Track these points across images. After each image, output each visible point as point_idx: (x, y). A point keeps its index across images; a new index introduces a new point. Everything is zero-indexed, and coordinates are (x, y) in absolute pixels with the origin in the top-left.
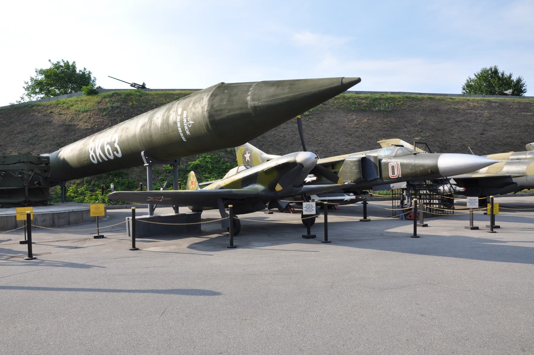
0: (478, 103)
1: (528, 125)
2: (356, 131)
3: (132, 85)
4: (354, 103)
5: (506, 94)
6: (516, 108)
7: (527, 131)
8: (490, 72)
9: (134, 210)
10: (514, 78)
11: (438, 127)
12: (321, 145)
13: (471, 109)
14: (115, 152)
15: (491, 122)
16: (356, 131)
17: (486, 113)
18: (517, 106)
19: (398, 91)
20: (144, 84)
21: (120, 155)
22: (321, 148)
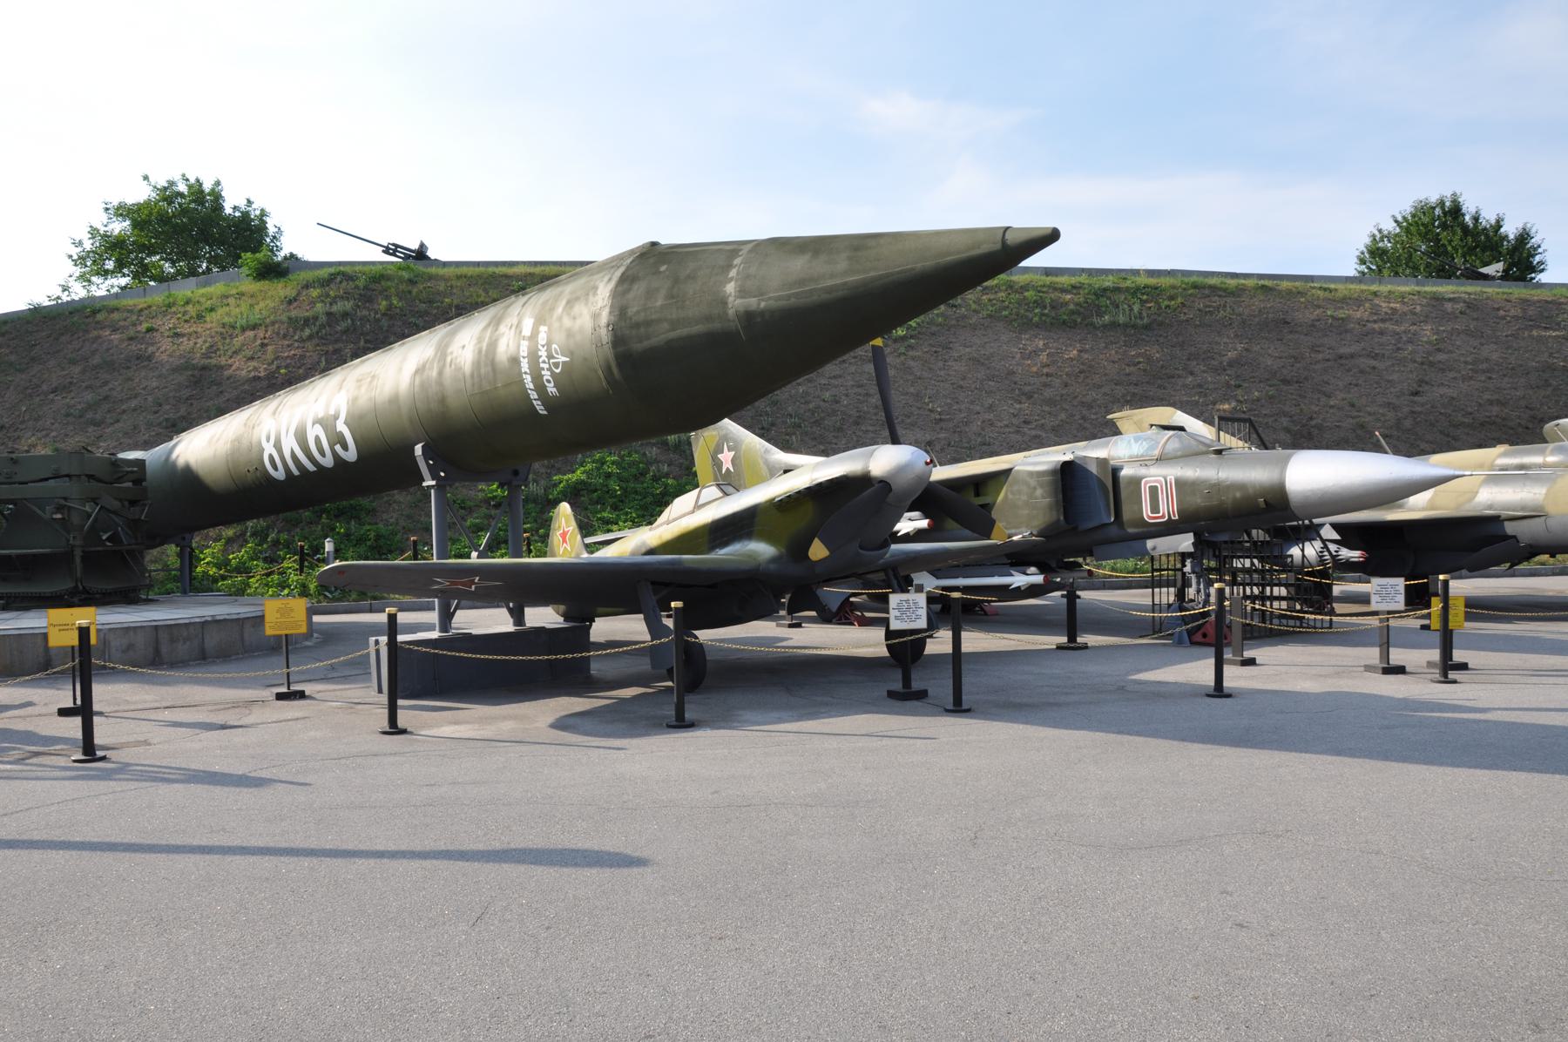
0: (1403, 303)
1: (1551, 368)
2: (1046, 385)
3: (387, 251)
4: (1039, 303)
5: (1486, 277)
6: (1516, 318)
7: (1547, 384)
8: (1438, 211)
9: (392, 618)
10: (1510, 230)
11: (1285, 371)
12: (943, 424)
13: (1383, 321)
14: (338, 448)
15: (1441, 357)
16: (1046, 385)
17: (1427, 332)
18: (1519, 312)
19: (1168, 267)
20: (422, 245)
21: (351, 455)
22: (942, 435)
